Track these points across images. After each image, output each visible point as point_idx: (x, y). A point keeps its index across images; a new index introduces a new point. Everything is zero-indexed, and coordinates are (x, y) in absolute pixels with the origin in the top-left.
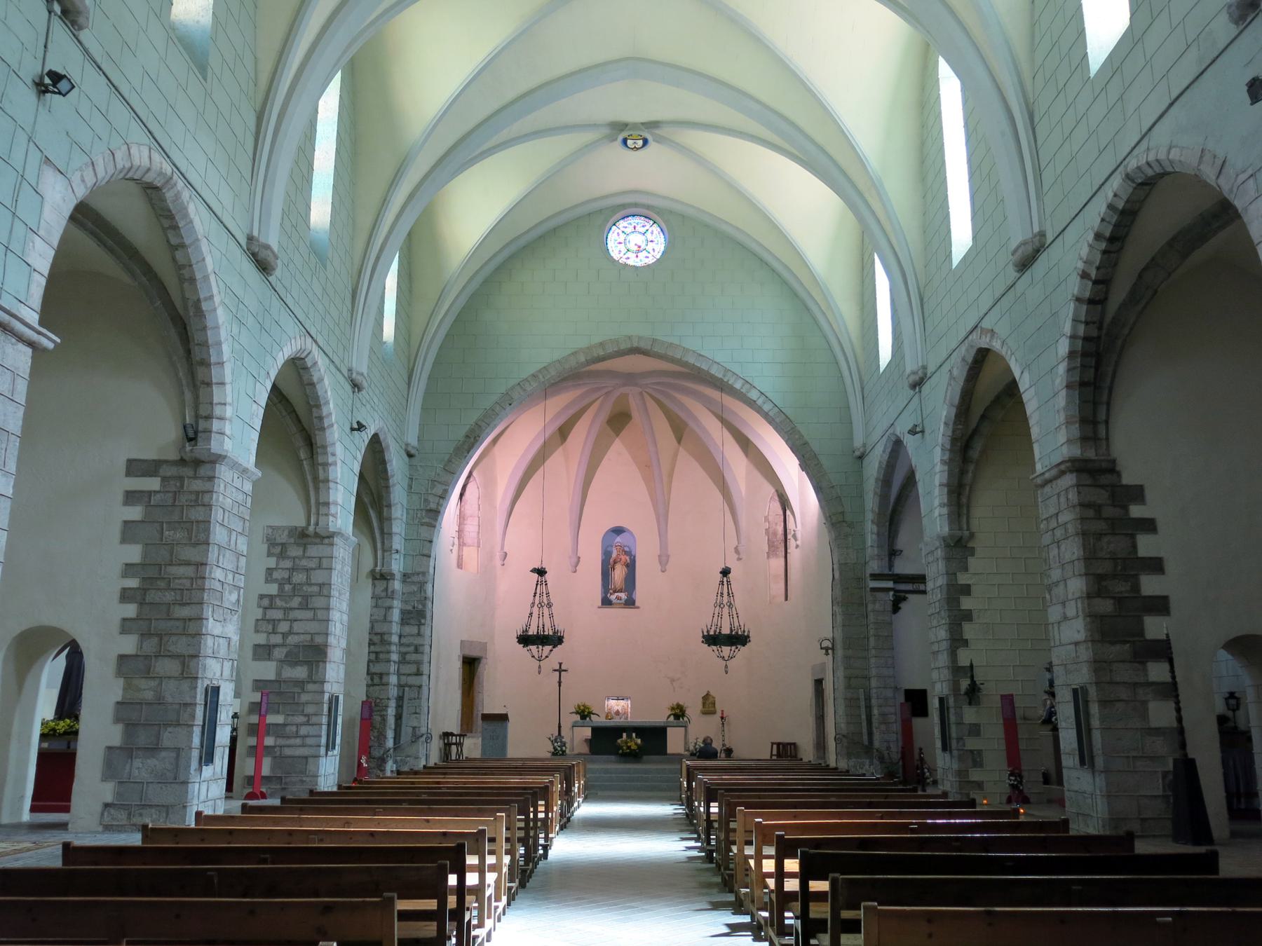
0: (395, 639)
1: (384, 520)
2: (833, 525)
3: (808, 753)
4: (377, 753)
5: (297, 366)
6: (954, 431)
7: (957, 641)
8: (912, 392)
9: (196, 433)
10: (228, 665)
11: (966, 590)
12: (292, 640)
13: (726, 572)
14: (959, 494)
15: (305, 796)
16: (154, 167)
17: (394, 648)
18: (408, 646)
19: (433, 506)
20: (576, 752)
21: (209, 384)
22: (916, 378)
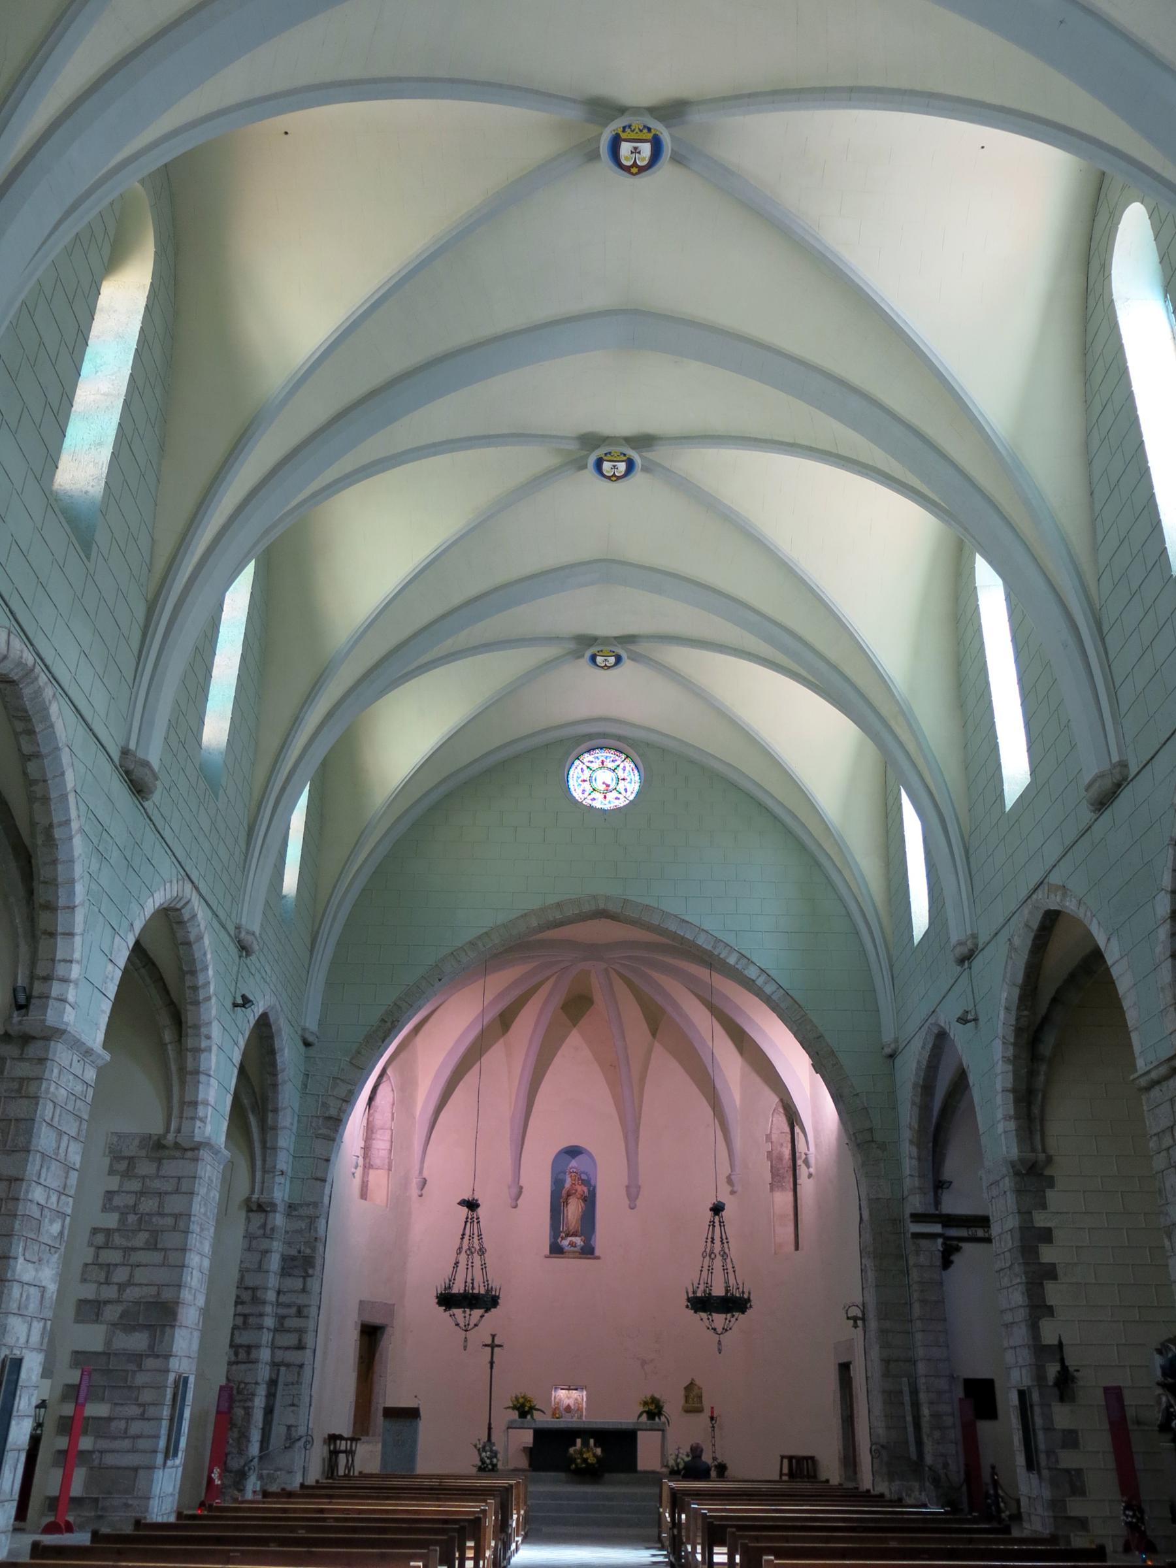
0: (271, 1296)
1: (267, 1129)
2: (858, 1145)
3: (831, 1471)
4: (235, 1464)
5: (170, 918)
6: (1017, 1019)
7: (1039, 1309)
8: (959, 968)
9: (29, 998)
10: (37, 1326)
11: (1046, 1235)
12: (132, 1294)
13: (717, 1209)
14: (1029, 1104)
15: (128, 1530)
16: (12, 655)
17: (268, 1309)
18: (289, 1306)
19: (333, 1112)
20: (511, 1467)
21: (52, 935)
22: (964, 950)
